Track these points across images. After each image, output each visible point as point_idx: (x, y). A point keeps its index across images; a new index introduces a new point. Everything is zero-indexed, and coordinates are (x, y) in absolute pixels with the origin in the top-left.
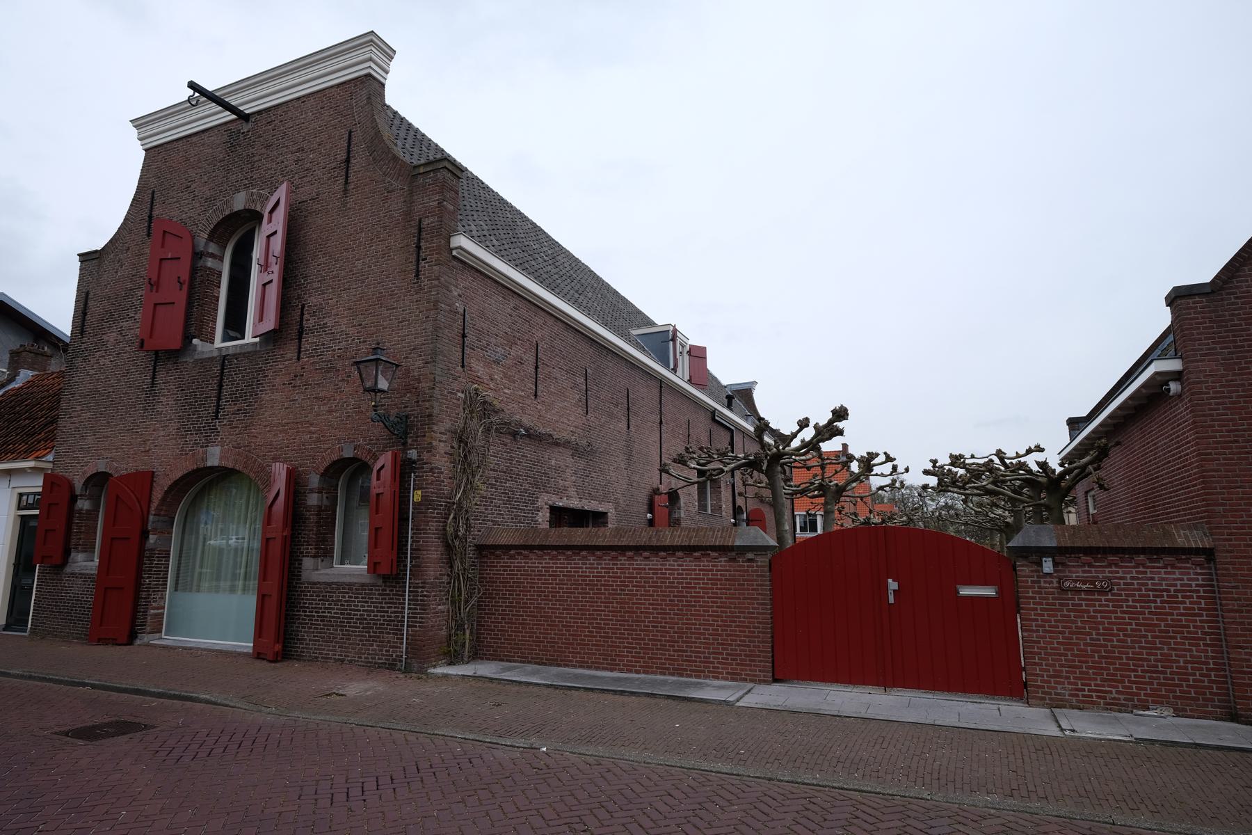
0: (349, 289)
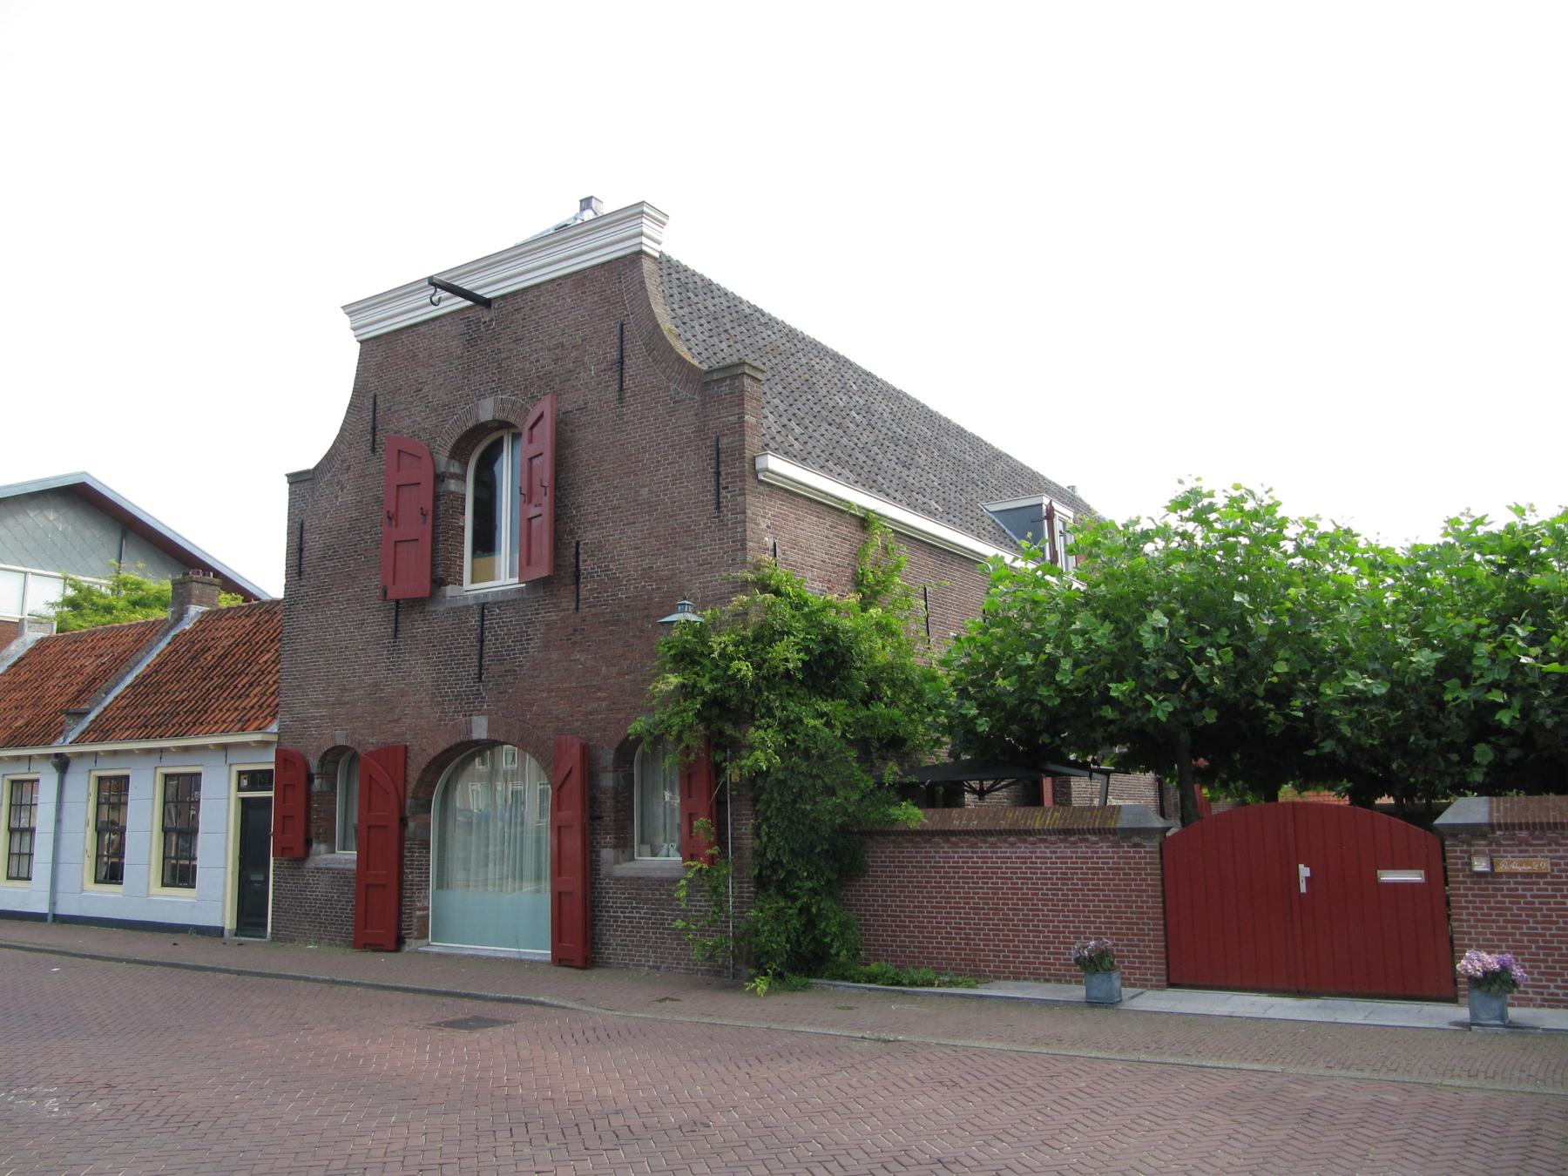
0: (634, 523)
